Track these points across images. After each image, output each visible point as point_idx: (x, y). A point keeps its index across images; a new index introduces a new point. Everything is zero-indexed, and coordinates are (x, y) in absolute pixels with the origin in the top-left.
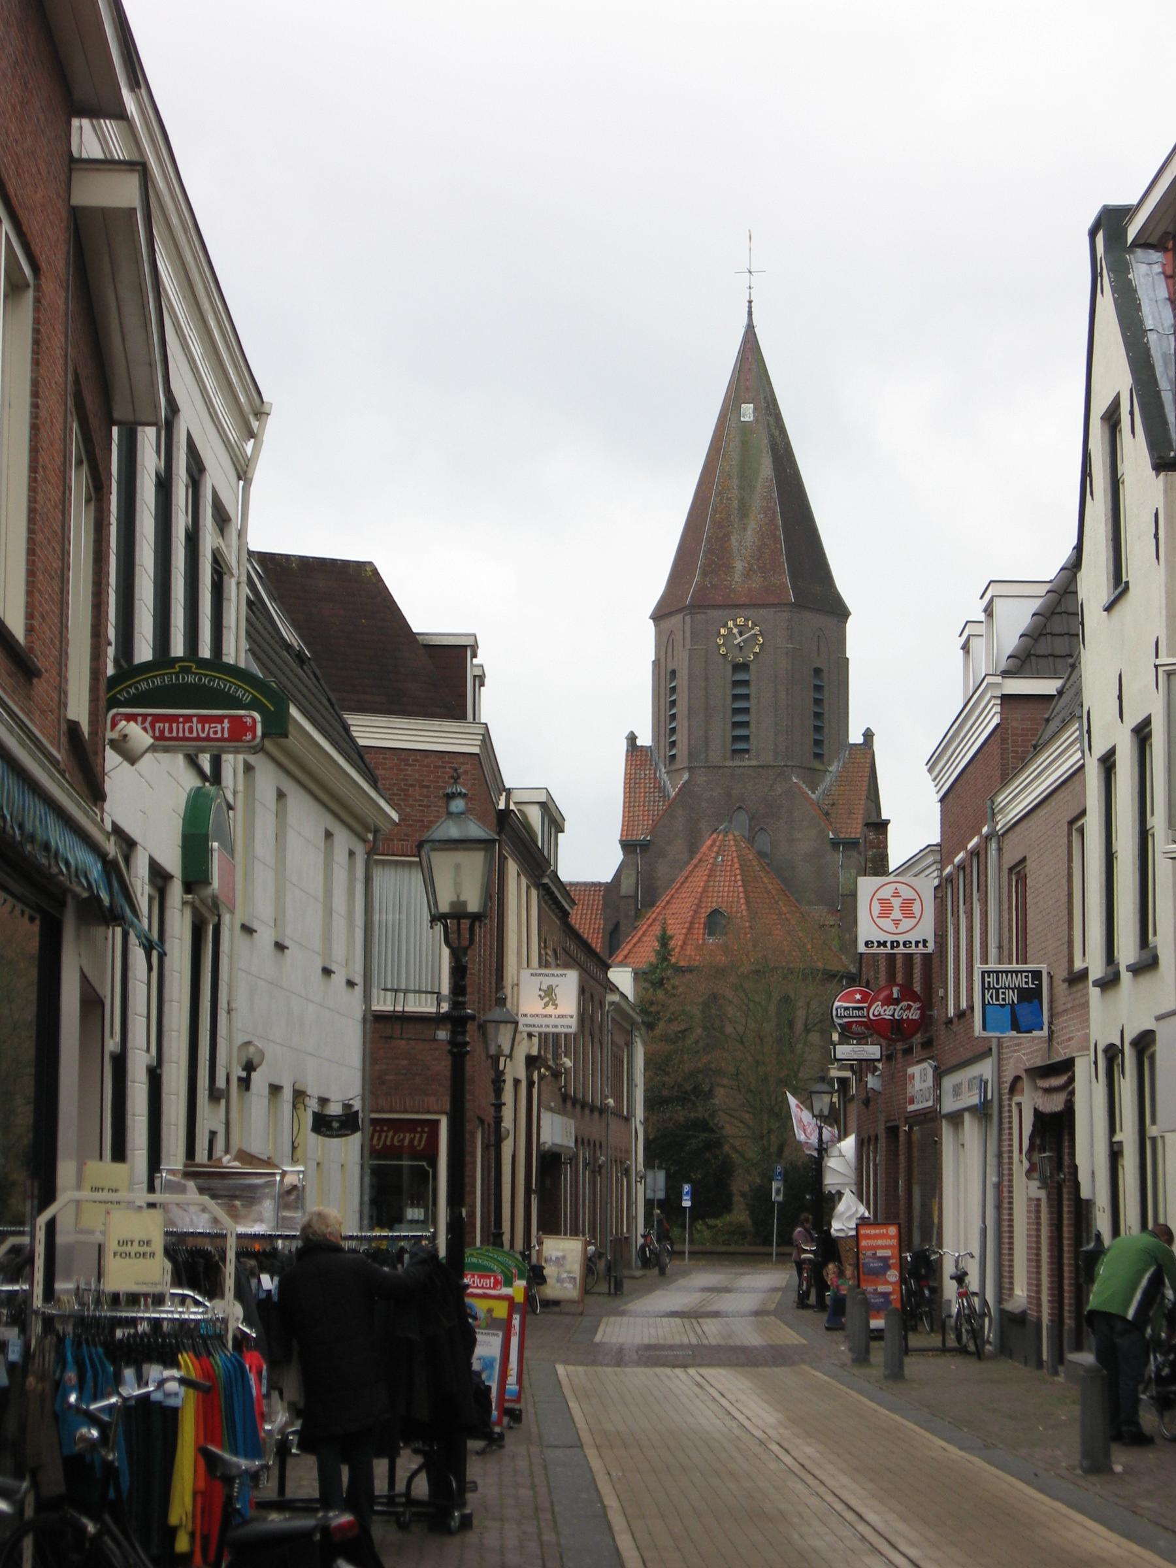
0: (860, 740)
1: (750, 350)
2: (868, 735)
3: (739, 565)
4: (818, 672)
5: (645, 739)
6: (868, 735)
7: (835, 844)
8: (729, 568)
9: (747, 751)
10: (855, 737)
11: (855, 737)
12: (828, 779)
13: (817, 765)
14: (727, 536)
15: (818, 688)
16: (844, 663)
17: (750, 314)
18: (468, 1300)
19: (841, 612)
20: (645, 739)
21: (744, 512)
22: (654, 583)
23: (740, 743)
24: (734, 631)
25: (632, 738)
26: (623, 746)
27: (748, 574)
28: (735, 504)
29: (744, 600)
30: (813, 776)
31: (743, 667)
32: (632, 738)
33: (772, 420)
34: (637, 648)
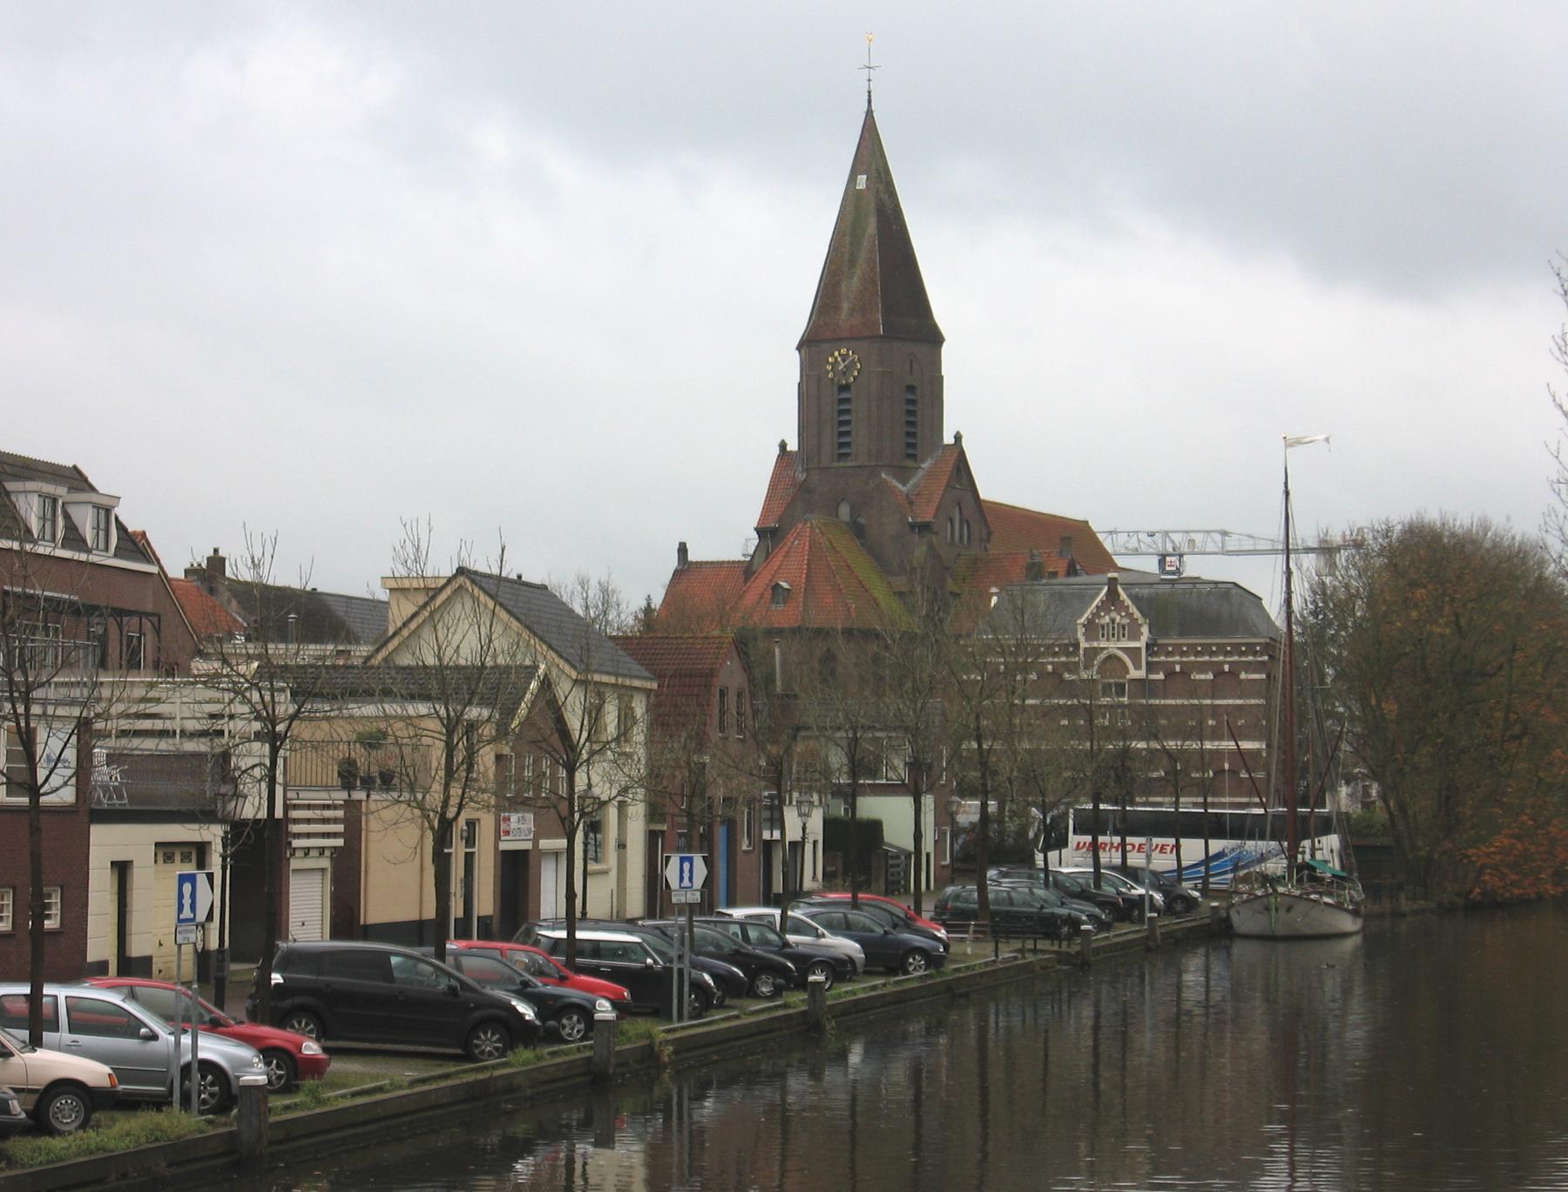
0: (952, 441)
1: (869, 130)
2: (958, 437)
3: (846, 306)
4: (911, 389)
5: (793, 446)
6: (958, 437)
7: (913, 526)
8: (838, 308)
9: (848, 455)
10: (948, 439)
11: (948, 439)
12: (920, 473)
13: (910, 463)
14: (838, 283)
15: (912, 402)
16: (939, 381)
17: (869, 102)
18: (1201, 951)
19: (934, 338)
20: (793, 446)
21: (852, 263)
22: (798, 323)
23: (843, 449)
24: (837, 357)
25: (783, 445)
26: (777, 451)
27: (852, 312)
28: (846, 257)
29: (846, 334)
30: (903, 474)
31: (845, 388)
32: (783, 445)
33: (881, 187)
34: (788, 370)
